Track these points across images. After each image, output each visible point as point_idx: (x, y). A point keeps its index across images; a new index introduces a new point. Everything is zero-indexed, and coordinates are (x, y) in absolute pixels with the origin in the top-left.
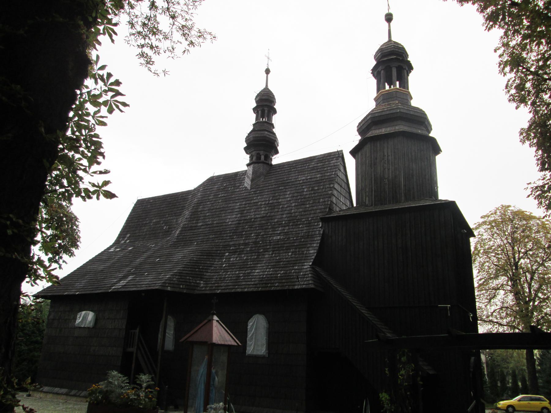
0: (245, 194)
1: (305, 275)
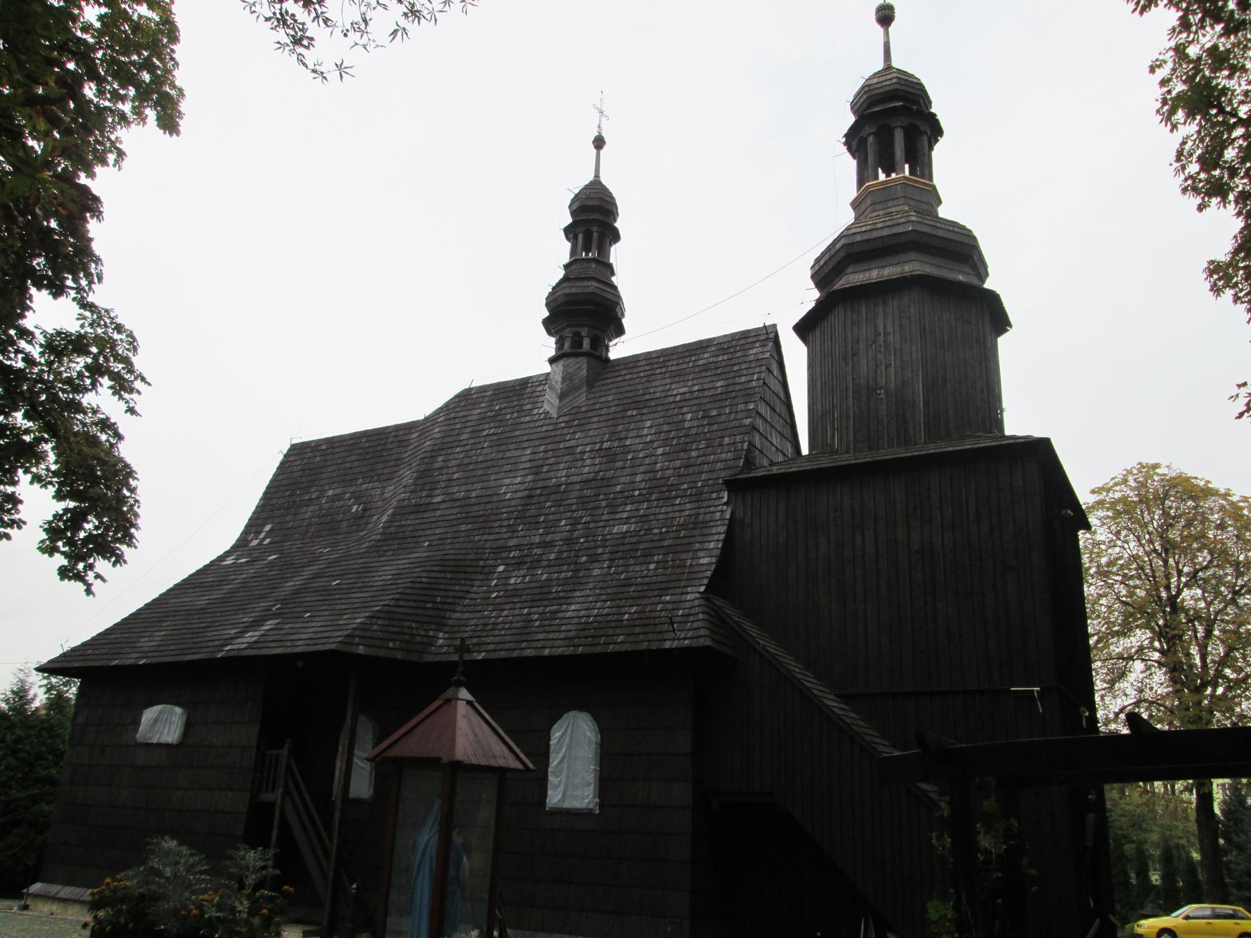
0: (545, 428)
1: (689, 615)
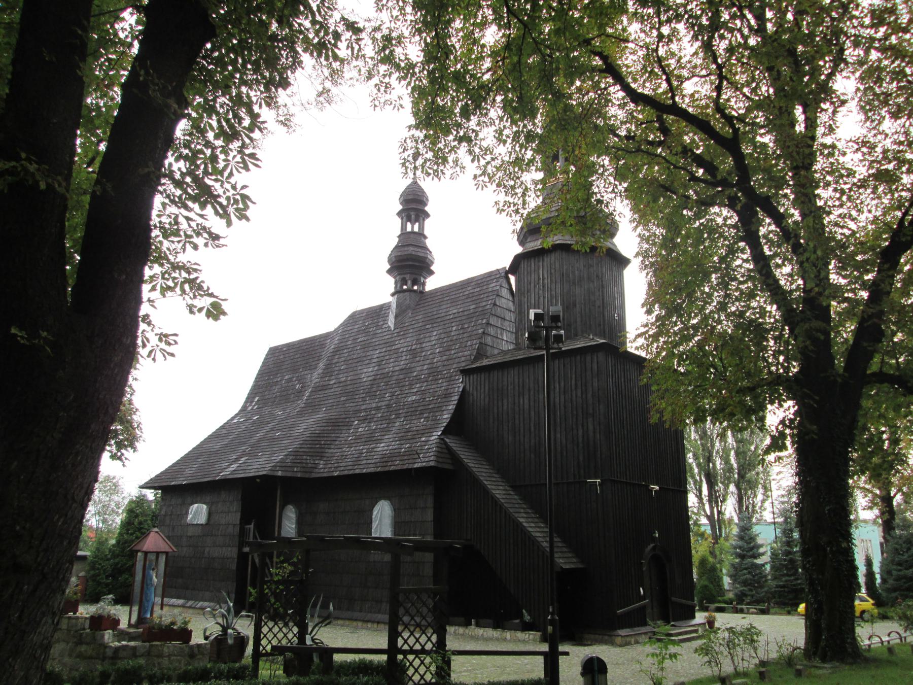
0: (387, 337)
